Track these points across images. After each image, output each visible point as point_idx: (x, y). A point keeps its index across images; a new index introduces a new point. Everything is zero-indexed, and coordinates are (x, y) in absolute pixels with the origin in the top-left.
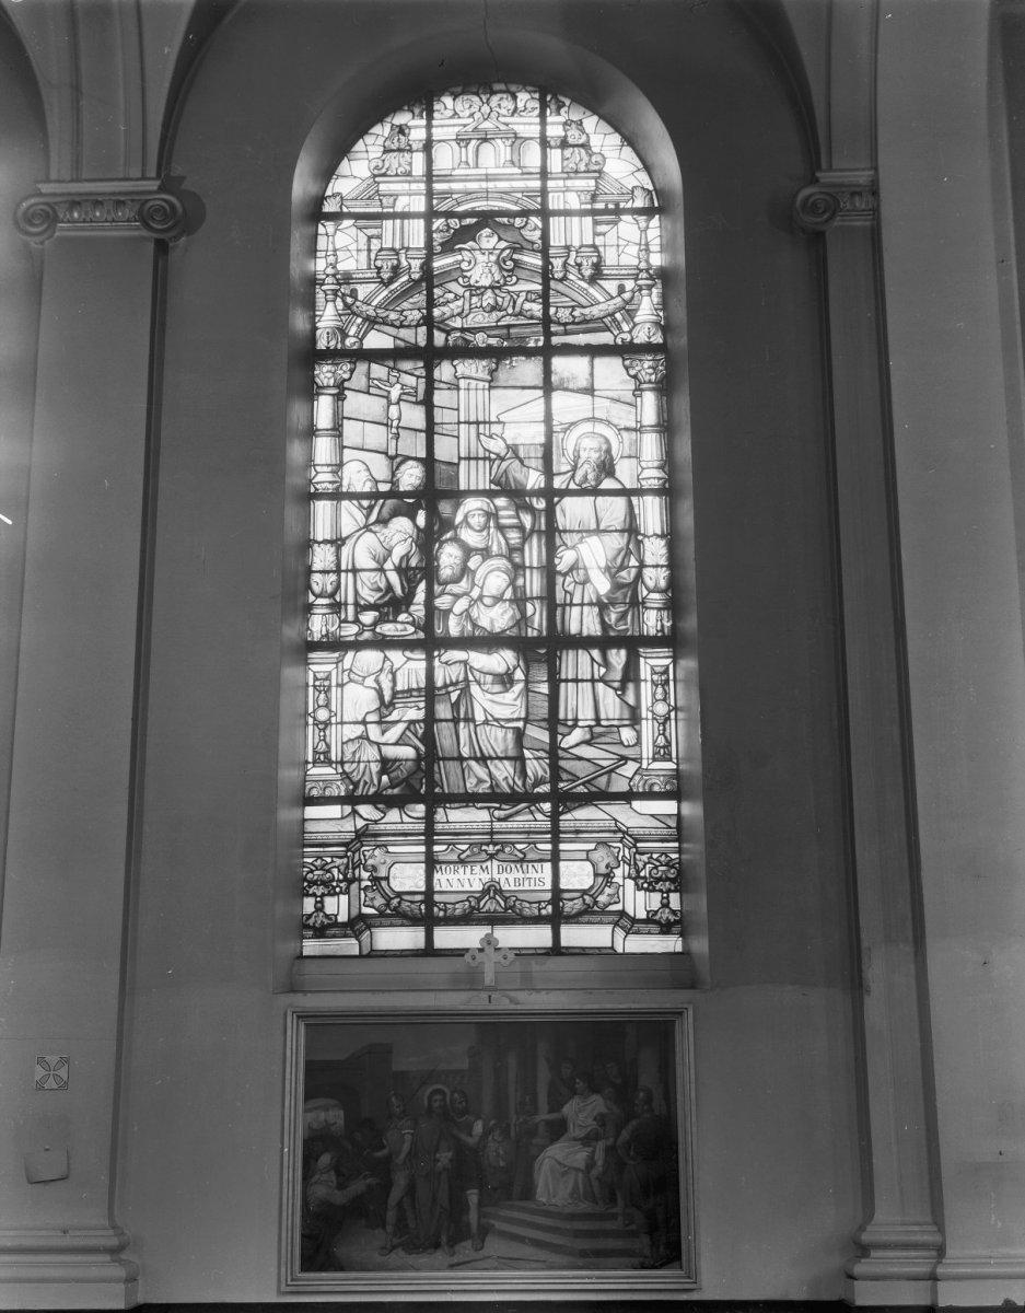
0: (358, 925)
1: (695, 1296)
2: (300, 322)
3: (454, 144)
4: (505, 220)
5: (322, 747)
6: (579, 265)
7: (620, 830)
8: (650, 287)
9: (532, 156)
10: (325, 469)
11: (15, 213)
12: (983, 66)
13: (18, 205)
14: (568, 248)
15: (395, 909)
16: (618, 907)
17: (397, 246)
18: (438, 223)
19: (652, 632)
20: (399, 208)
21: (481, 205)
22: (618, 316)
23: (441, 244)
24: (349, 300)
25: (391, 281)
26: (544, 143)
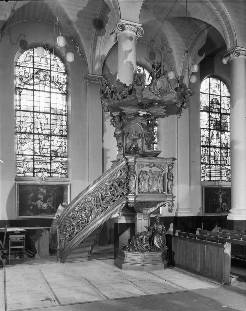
0: (24, 172)
1: (162, 216)
2: (15, 82)
3: (37, 57)
4: (45, 71)
5: (65, 150)
6: (55, 80)
7: (59, 161)
8: (65, 85)
9: (49, 61)
10: (18, 106)
11: (85, 76)
12: (86, 53)
13: (85, 76)
14: (53, 77)
15: (29, 170)
16: (59, 172)
17: (29, 72)
18: (35, 70)
19: (64, 135)
20: (29, 66)
21: (41, 68)
22: (60, 88)
23: (35, 73)
24: (21, 80)
25: (28, 78)
26: (50, 59)
